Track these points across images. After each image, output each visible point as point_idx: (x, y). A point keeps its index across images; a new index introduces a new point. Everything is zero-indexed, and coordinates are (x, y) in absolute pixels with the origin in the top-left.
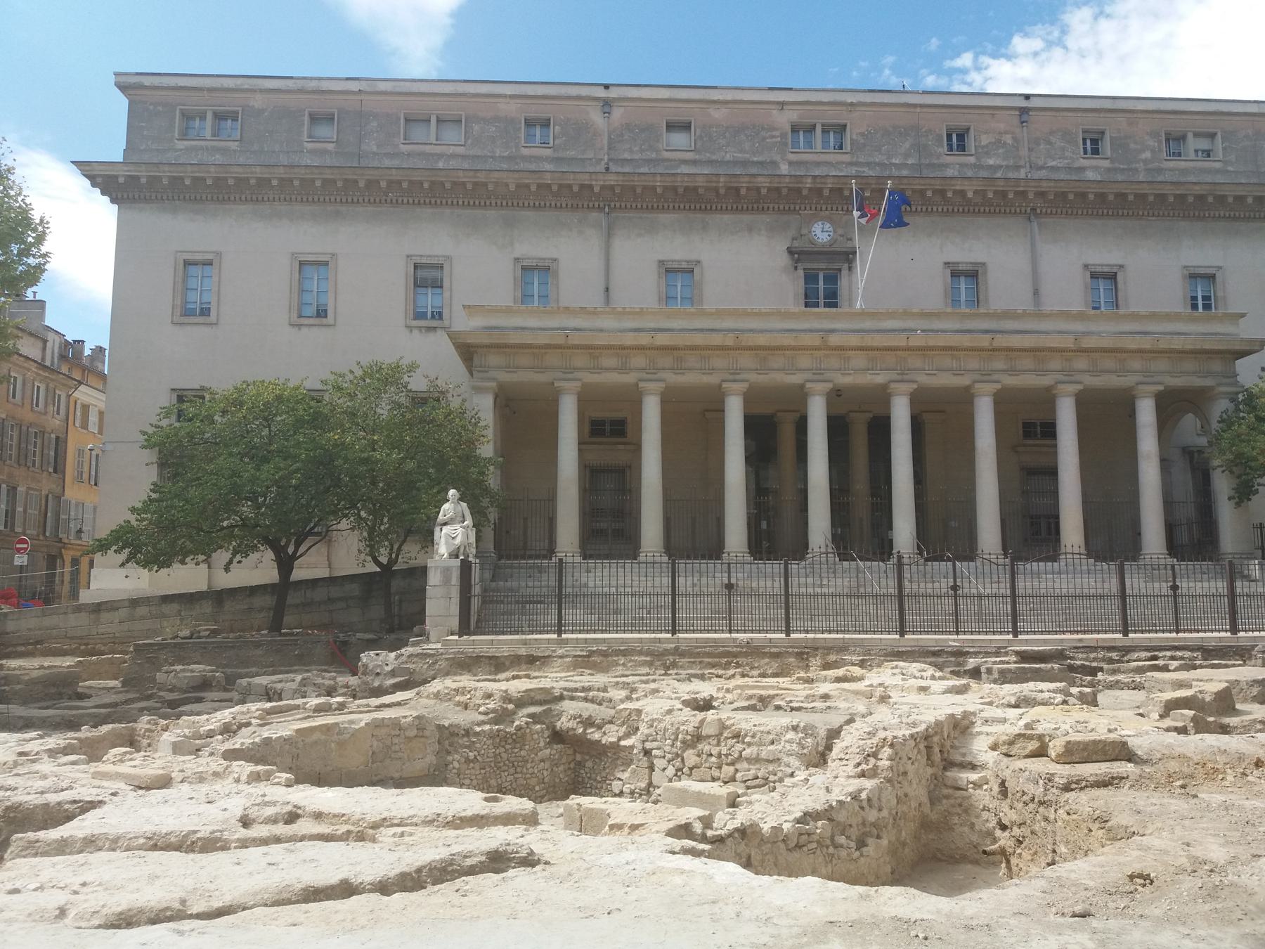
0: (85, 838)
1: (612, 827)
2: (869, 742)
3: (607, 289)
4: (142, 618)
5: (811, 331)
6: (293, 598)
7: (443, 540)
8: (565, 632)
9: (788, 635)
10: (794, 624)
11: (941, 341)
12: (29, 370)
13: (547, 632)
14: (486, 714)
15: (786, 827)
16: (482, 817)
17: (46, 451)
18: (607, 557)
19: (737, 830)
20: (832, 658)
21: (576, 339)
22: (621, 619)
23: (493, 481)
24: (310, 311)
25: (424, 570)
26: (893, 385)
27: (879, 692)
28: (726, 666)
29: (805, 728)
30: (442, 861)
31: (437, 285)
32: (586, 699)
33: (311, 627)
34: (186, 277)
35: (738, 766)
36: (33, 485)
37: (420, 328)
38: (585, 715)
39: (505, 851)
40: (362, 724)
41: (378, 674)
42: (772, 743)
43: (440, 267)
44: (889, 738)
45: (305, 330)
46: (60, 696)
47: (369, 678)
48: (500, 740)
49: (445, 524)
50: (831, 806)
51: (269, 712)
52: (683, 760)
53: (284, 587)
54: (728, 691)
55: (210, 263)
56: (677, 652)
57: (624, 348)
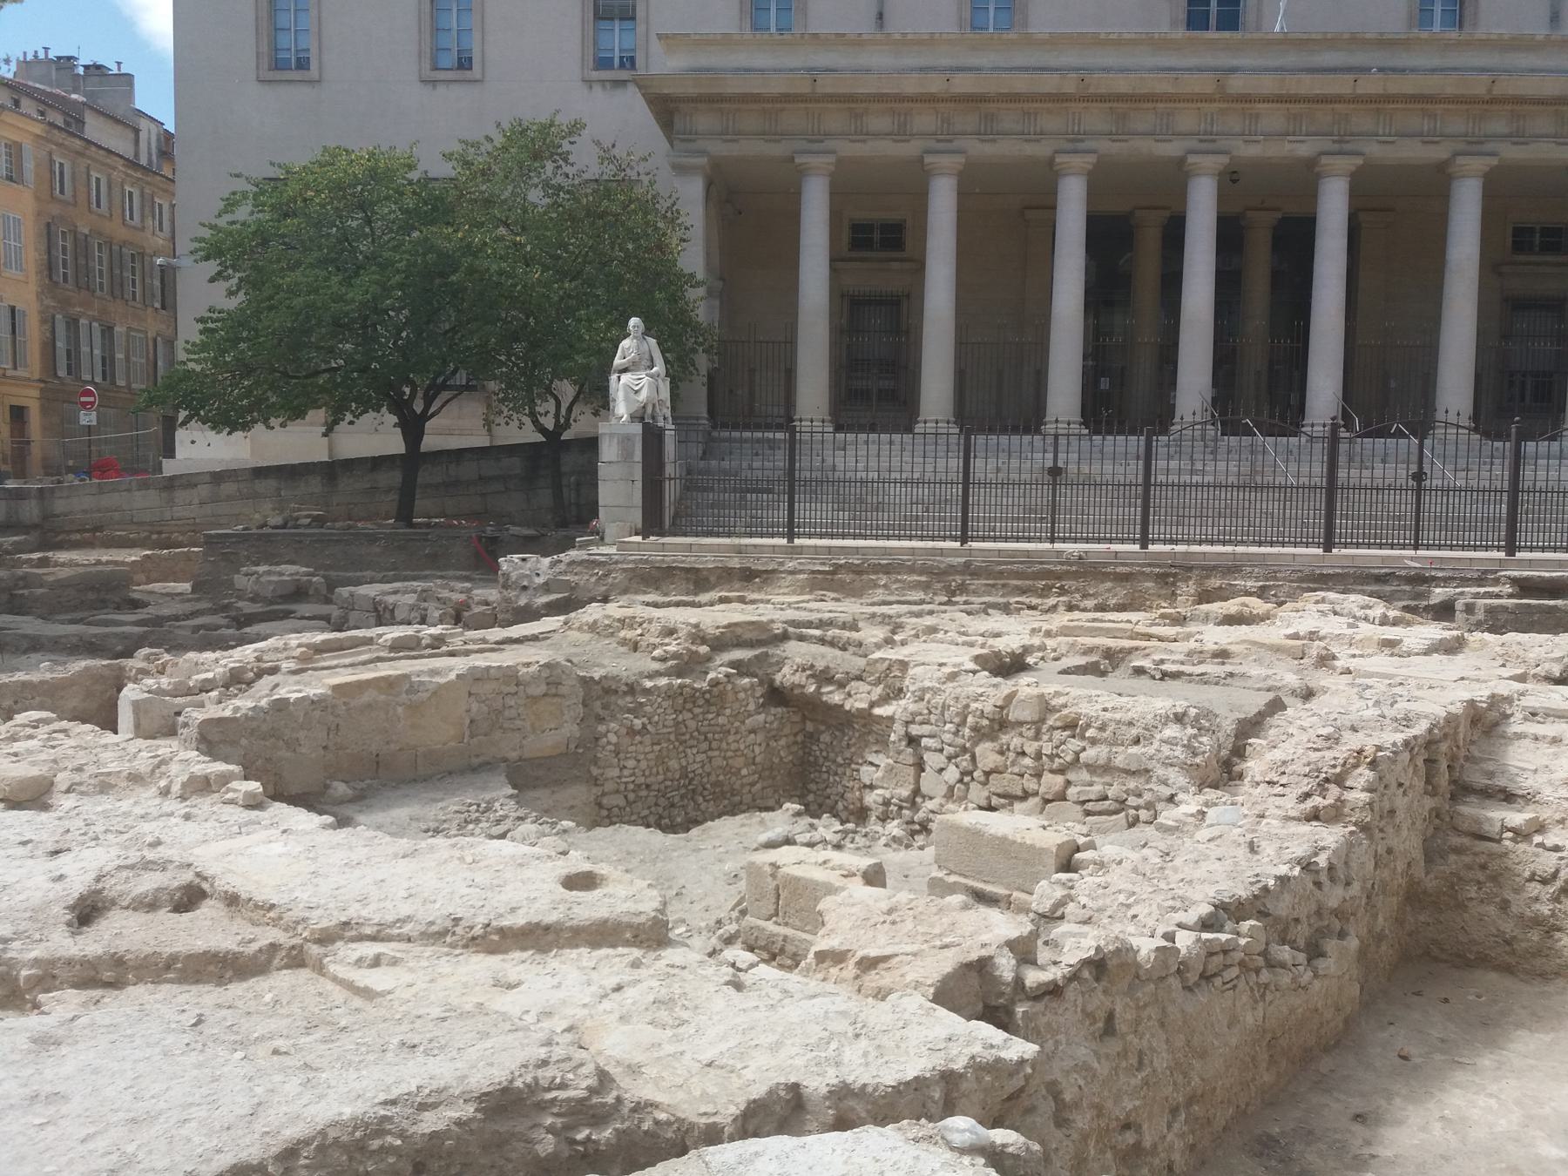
1: (821, 957)
2: (1328, 754)
3: (880, 16)
4: (229, 498)
5: (1200, 70)
6: (424, 476)
8: (799, 536)
9: (1144, 546)
10: (1154, 531)
11: (1408, 85)
12: (114, 168)
13: (772, 536)
15: (1185, 941)
16: (547, 928)
17: (148, 280)
18: (872, 429)
19: (1086, 962)
20: (1215, 582)
21: (827, 85)
22: (884, 518)
23: (702, 308)
24: (449, 60)
26: (1324, 160)
27: (1315, 648)
28: (1044, 593)
29: (1197, 718)
30: (356, 1123)
32: (822, 641)
35: (1071, 776)
36: (135, 325)
38: (820, 665)
39: (534, 1087)
40: (452, 676)
41: (525, 588)
42: (1137, 741)
44: (1369, 750)
45: (441, 89)
46: (102, 604)
48: (684, 700)
49: (625, 370)
50: (1265, 889)
51: (320, 649)
52: (973, 758)
53: (413, 459)
54: (1048, 634)
56: (968, 569)
57: (900, 98)
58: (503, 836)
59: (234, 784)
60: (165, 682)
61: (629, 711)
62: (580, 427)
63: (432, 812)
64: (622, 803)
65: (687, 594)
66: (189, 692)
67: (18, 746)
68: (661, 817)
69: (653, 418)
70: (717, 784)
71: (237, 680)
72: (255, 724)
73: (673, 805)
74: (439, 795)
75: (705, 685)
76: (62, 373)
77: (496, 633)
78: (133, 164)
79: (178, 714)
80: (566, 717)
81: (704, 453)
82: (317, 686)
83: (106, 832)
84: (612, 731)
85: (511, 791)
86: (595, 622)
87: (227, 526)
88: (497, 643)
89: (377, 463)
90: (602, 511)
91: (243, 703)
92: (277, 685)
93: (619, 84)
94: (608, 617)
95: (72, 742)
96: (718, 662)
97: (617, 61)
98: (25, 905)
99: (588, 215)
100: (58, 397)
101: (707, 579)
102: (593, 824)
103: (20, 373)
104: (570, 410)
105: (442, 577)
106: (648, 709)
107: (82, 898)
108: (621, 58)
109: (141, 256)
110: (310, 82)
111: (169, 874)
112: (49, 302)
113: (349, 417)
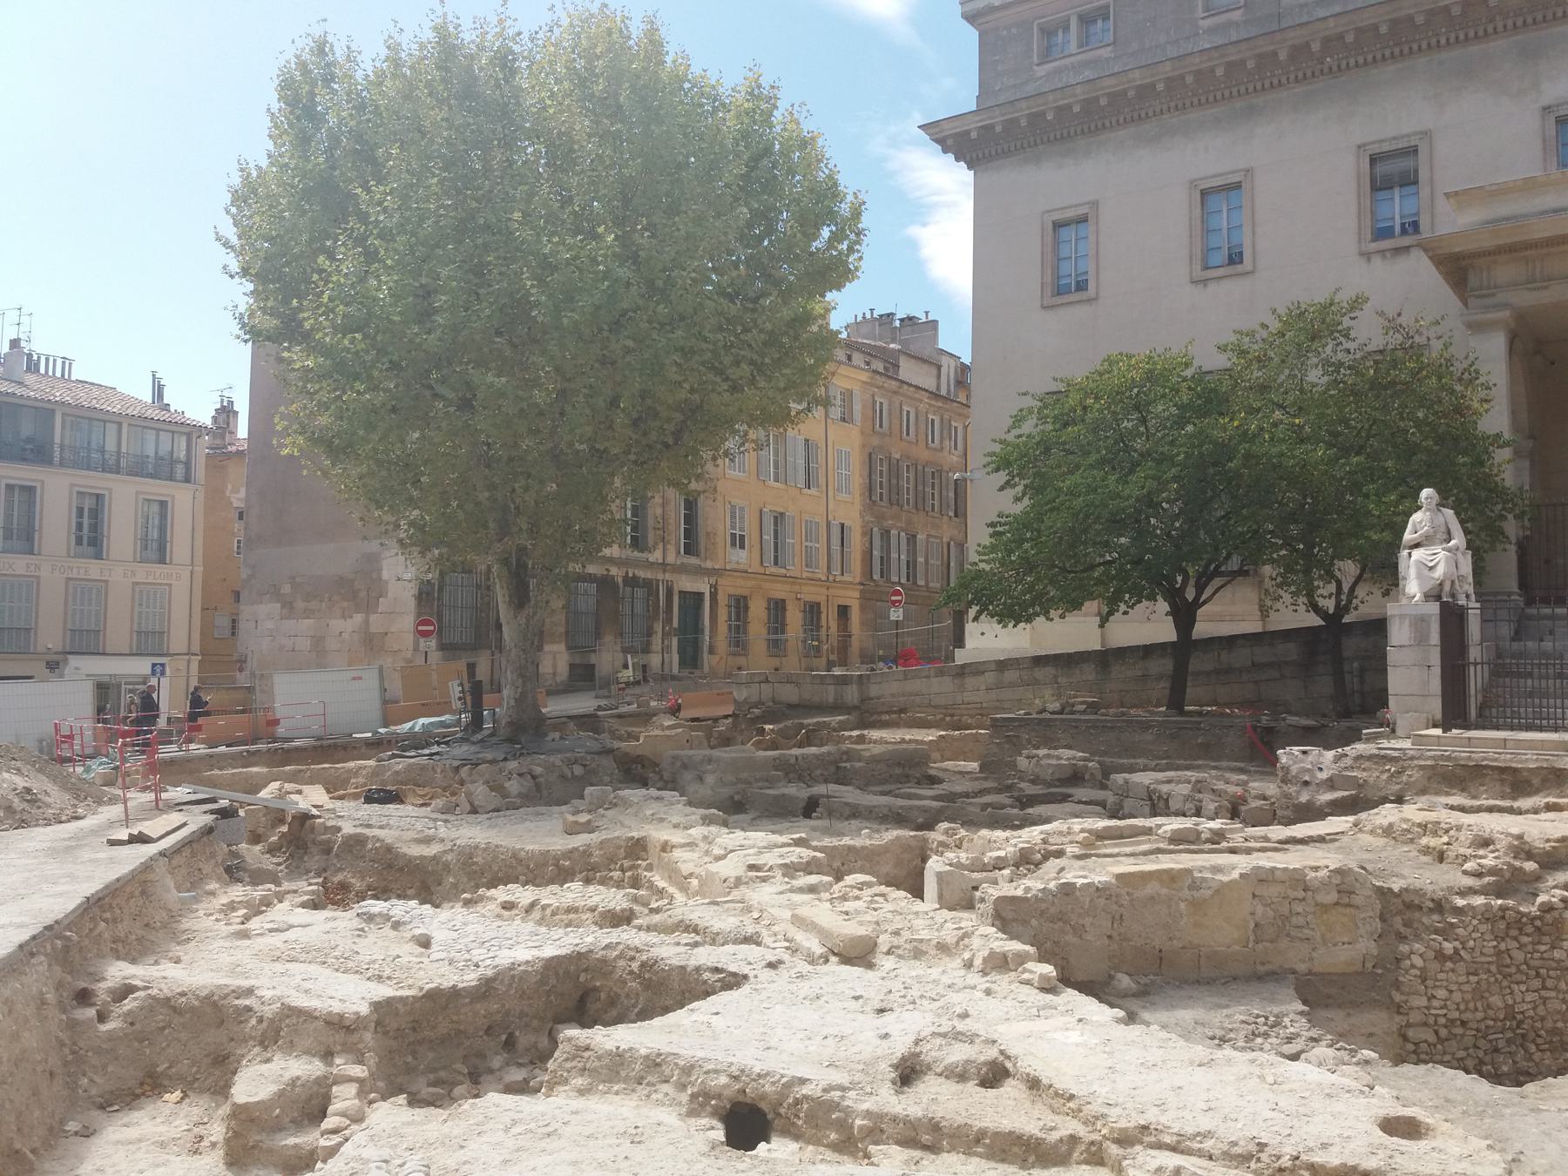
0: (647, 1057)
4: (1012, 685)
6: (1195, 664)
7: (1412, 572)
14: (1478, 875)
23: (1508, 469)
24: (1220, 257)
25: (1378, 627)
31: (1409, 180)
33: (1230, 705)
34: (1057, 243)
36: (933, 533)
37: (1382, 252)
40: (1235, 875)
41: (1306, 783)
43: (1414, 151)
45: (1212, 286)
46: (906, 778)
47: (1292, 789)
49: (1417, 546)
51: (1101, 835)
53: (1184, 647)
55: (1083, 220)
58: (1294, 1057)
59: (1030, 965)
60: (963, 856)
61: (1436, 932)
62: (1367, 605)
63: (1218, 1019)
64: (1432, 1038)
65: (1503, 798)
66: (984, 868)
67: (849, 906)
68: (1482, 1062)
69: (1453, 595)
70: (1554, 1031)
71: (1026, 861)
72: (1044, 906)
73: (1496, 1050)
74: (1224, 1001)
75: (1533, 910)
76: (876, 577)
77: (1278, 832)
78: (936, 395)
79: (976, 888)
80: (1362, 931)
81: (1517, 632)
82: (1100, 872)
83: (922, 997)
84: (1416, 953)
85: (1302, 1008)
86: (1391, 825)
87: (1009, 711)
88: (1280, 842)
89: (1148, 651)
90: (1392, 702)
91: (1032, 884)
92: (1062, 869)
93: (1406, 249)
94: (1406, 820)
95: (889, 907)
96: (1550, 883)
97: (1398, 229)
98: (858, 1057)
99: (1371, 389)
100: (873, 596)
101: (1528, 782)
102: (1399, 1060)
103: (847, 578)
104: (1352, 589)
105: (1215, 768)
106: (1460, 931)
107: (904, 1059)
108: (1403, 225)
109: (939, 473)
110: (1089, 301)
111: (976, 1048)
112: (869, 518)
113: (1123, 607)
